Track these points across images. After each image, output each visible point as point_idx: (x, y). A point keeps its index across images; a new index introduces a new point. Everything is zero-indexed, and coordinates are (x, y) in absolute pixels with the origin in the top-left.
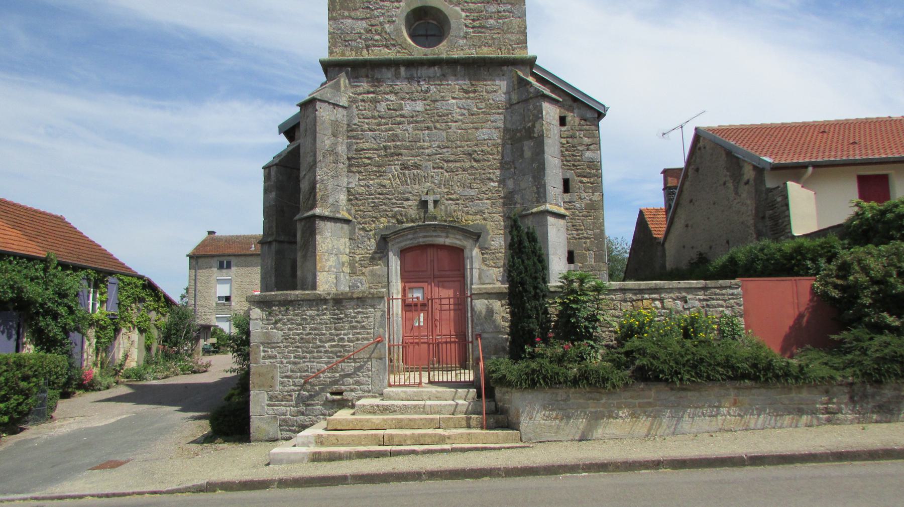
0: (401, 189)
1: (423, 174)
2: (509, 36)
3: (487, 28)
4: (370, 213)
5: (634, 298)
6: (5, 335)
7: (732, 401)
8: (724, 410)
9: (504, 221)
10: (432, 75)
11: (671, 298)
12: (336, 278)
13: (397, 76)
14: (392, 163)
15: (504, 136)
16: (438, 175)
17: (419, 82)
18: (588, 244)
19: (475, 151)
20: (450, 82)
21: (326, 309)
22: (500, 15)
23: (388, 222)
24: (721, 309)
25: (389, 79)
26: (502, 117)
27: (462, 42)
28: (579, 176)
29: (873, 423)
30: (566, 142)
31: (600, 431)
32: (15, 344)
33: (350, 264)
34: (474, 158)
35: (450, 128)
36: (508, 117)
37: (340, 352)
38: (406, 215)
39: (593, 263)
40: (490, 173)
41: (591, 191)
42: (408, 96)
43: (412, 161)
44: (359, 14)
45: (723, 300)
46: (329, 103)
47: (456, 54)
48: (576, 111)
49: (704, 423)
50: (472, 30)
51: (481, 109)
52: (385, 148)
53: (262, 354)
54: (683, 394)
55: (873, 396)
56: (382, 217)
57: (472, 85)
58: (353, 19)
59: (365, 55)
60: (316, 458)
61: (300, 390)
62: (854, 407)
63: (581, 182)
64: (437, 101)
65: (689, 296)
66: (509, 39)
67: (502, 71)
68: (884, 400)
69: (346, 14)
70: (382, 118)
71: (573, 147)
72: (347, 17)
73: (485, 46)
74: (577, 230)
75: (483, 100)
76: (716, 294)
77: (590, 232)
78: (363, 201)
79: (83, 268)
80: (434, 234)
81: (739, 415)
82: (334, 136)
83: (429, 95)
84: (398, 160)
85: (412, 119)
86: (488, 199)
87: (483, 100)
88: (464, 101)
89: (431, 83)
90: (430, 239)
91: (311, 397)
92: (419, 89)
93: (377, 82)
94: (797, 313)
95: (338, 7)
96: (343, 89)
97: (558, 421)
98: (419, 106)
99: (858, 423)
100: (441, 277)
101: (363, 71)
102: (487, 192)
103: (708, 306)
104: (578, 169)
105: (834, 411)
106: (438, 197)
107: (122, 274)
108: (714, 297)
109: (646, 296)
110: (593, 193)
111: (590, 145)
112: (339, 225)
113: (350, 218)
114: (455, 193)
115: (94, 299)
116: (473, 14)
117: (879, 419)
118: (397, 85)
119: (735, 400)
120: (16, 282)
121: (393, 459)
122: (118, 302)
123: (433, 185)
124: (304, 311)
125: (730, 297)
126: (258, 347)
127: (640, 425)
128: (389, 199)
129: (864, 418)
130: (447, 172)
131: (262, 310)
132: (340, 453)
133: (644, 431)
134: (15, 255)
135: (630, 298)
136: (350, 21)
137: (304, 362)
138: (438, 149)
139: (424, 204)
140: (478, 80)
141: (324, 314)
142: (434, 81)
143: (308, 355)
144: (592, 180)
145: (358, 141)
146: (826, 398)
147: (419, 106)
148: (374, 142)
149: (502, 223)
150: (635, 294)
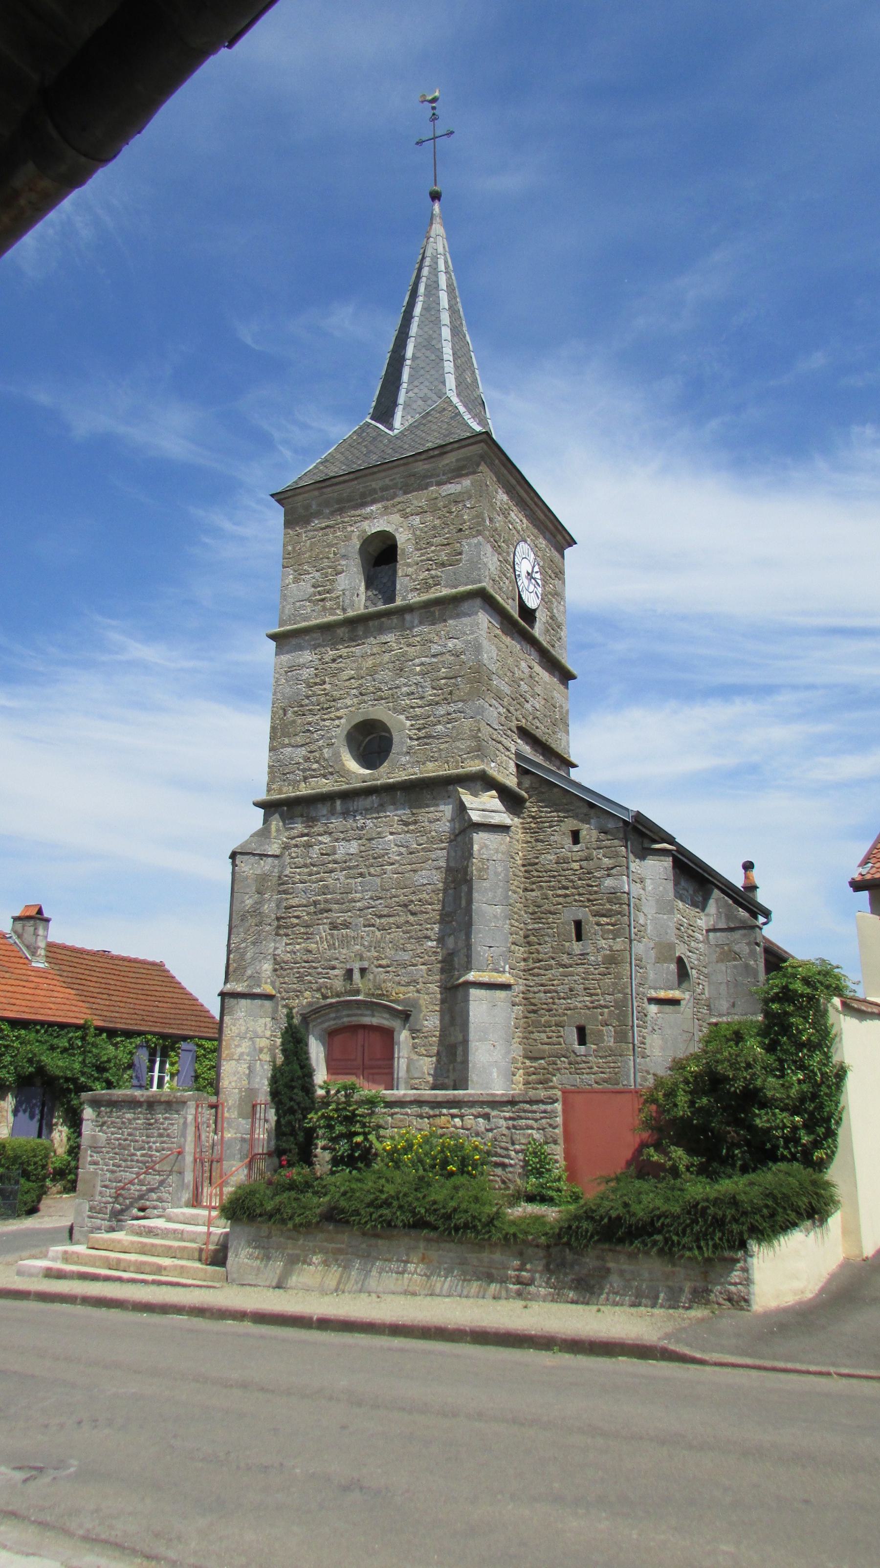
0: (329, 953)
1: (352, 934)
2: (458, 744)
3: (434, 737)
4: (295, 986)
5: (431, 1112)
6: (27, 1114)
7: (421, 1255)
8: (411, 1267)
9: (441, 993)
10: (368, 807)
11: (473, 1115)
12: (249, 1068)
13: (333, 812)
14: (320, 922)
15: (446, 878)
16: (368, 935)
17: (355, 816)
18: (606, 1015)
19: (412, 901)
20: (388, 814)
21: (140, 1113)
22: (449, 717)
23: (313, 997)
24: (530, 1131)
25: (324, 816)
26: (445, 852)
27: (404, 759)
28: (595, 916)
29: (568, 1302)
30: (578, 867)
31: (294, 1278)
32: (37, 1125)
33: (270, 1050)
34: (409, 911)
35: (385, 873)
36: (453, 854)
37: (148, 1162)
38: (331, 988)
39: (611, 1044)
40: (427, 929)
41: (611, 937)
42: (342, 836)
43: (341, 918)
44: (299, 740)
45: (533, 1119)
46: (254, 855)
47: (400, 776)
48: (592, 821)
49: (390, 1281)
50: (416, 742)
51: (422, 844)
52: (315, 903)
53: (89, 1159)
54: (373, 1241)
55: (572, 1266)
56: (306, 990)
57: (413, 814)
58: (293, 746)
59: (304, 790)
60: (51, 1274)
61: (113, 1203)
62: (549, 1279)
63: (598, 924)
64: (372, 839)
65: (494, 1113)
66: (458, 748)
67: (447, 791)
68: (585, 1271)
69: (286, 741)
70: (314, 866)
71: (588, 873)
72: (285, 746)
73: (431, 761)
74: (591, 995)
75: (425, 833)
76: (525, 1111)
77: (608, 997)
78: (288, 971)
79: (139, 1034)
80: (359, 1012)
81: (425, 1275)
82: (259, 893)
83: (364, 832)
84: (327, 918)
85: (345, 865)
86: (423, 964)
87: (425, 833)
88: (402, 836)
89: (368, 816)
90: (354, 1019)
91: (122, 1212)
92: (355, 825)
93: (310, 820)
94: (638, 1140)
95: (279, 734)
96: (274, 834)
97: (259, 1262)
98: (354, 847)
99: (552, 1301)
100: (371, 1068)
101: (298, 810)
102: (422, 955)
103: (514, 1127)
104: (594, 905)
105: (525, 1281)
106: (366, 964)
107: (200, 1038)
108: (522, 1114)
109: (445, 1111)
110: (614, 939)
111: (612, 868)
112: (258, 1002)
113: (274, 992)
114: (386, 957)
115: (161, 1070)
116: (418, 722)
117: (575, 1298)
118: (331, 823)
119: (423, 1254)
120: (35, 1055)
121: (106, 1284)
122: (193, 1074)
123: (363, 949)
124: (124, 1113)
125: (542, 1115)
126: (86, 1150)
127: (331, 1275)
128: (315, 968)
129: (558, 1294)
130: (379, 930)
131: (94, 1111)
132: (65, 1272)
133: (333, 1284)
134: (42, 1023)
135: (427, 1113)
136: (289, 749)
137: (120, 1171)
138: (370, 901)
139: (349, 973)
140: (420, 807)
141: (138, 1119)
142: (371, 813)
143: (123, 1164)
144: (613, 920)
145: (288, 896)
146: (519, 1263)
147: (354, 847)
148: (304, 897)
149: (439, 996)
150: (432, 1108)
